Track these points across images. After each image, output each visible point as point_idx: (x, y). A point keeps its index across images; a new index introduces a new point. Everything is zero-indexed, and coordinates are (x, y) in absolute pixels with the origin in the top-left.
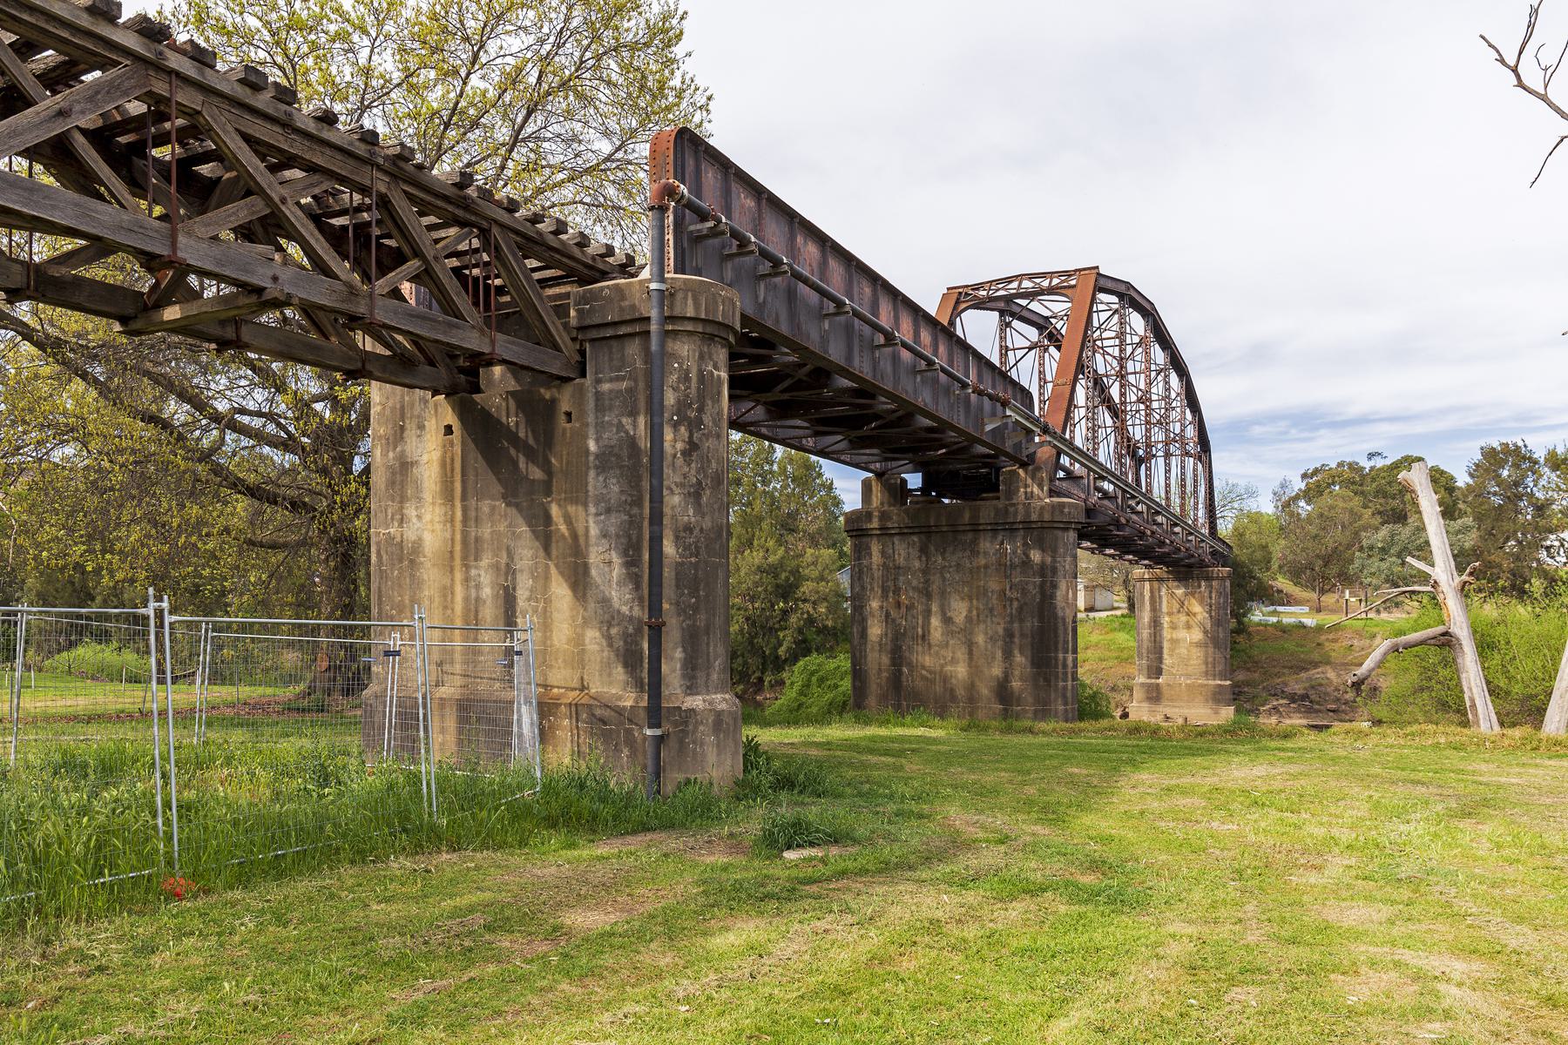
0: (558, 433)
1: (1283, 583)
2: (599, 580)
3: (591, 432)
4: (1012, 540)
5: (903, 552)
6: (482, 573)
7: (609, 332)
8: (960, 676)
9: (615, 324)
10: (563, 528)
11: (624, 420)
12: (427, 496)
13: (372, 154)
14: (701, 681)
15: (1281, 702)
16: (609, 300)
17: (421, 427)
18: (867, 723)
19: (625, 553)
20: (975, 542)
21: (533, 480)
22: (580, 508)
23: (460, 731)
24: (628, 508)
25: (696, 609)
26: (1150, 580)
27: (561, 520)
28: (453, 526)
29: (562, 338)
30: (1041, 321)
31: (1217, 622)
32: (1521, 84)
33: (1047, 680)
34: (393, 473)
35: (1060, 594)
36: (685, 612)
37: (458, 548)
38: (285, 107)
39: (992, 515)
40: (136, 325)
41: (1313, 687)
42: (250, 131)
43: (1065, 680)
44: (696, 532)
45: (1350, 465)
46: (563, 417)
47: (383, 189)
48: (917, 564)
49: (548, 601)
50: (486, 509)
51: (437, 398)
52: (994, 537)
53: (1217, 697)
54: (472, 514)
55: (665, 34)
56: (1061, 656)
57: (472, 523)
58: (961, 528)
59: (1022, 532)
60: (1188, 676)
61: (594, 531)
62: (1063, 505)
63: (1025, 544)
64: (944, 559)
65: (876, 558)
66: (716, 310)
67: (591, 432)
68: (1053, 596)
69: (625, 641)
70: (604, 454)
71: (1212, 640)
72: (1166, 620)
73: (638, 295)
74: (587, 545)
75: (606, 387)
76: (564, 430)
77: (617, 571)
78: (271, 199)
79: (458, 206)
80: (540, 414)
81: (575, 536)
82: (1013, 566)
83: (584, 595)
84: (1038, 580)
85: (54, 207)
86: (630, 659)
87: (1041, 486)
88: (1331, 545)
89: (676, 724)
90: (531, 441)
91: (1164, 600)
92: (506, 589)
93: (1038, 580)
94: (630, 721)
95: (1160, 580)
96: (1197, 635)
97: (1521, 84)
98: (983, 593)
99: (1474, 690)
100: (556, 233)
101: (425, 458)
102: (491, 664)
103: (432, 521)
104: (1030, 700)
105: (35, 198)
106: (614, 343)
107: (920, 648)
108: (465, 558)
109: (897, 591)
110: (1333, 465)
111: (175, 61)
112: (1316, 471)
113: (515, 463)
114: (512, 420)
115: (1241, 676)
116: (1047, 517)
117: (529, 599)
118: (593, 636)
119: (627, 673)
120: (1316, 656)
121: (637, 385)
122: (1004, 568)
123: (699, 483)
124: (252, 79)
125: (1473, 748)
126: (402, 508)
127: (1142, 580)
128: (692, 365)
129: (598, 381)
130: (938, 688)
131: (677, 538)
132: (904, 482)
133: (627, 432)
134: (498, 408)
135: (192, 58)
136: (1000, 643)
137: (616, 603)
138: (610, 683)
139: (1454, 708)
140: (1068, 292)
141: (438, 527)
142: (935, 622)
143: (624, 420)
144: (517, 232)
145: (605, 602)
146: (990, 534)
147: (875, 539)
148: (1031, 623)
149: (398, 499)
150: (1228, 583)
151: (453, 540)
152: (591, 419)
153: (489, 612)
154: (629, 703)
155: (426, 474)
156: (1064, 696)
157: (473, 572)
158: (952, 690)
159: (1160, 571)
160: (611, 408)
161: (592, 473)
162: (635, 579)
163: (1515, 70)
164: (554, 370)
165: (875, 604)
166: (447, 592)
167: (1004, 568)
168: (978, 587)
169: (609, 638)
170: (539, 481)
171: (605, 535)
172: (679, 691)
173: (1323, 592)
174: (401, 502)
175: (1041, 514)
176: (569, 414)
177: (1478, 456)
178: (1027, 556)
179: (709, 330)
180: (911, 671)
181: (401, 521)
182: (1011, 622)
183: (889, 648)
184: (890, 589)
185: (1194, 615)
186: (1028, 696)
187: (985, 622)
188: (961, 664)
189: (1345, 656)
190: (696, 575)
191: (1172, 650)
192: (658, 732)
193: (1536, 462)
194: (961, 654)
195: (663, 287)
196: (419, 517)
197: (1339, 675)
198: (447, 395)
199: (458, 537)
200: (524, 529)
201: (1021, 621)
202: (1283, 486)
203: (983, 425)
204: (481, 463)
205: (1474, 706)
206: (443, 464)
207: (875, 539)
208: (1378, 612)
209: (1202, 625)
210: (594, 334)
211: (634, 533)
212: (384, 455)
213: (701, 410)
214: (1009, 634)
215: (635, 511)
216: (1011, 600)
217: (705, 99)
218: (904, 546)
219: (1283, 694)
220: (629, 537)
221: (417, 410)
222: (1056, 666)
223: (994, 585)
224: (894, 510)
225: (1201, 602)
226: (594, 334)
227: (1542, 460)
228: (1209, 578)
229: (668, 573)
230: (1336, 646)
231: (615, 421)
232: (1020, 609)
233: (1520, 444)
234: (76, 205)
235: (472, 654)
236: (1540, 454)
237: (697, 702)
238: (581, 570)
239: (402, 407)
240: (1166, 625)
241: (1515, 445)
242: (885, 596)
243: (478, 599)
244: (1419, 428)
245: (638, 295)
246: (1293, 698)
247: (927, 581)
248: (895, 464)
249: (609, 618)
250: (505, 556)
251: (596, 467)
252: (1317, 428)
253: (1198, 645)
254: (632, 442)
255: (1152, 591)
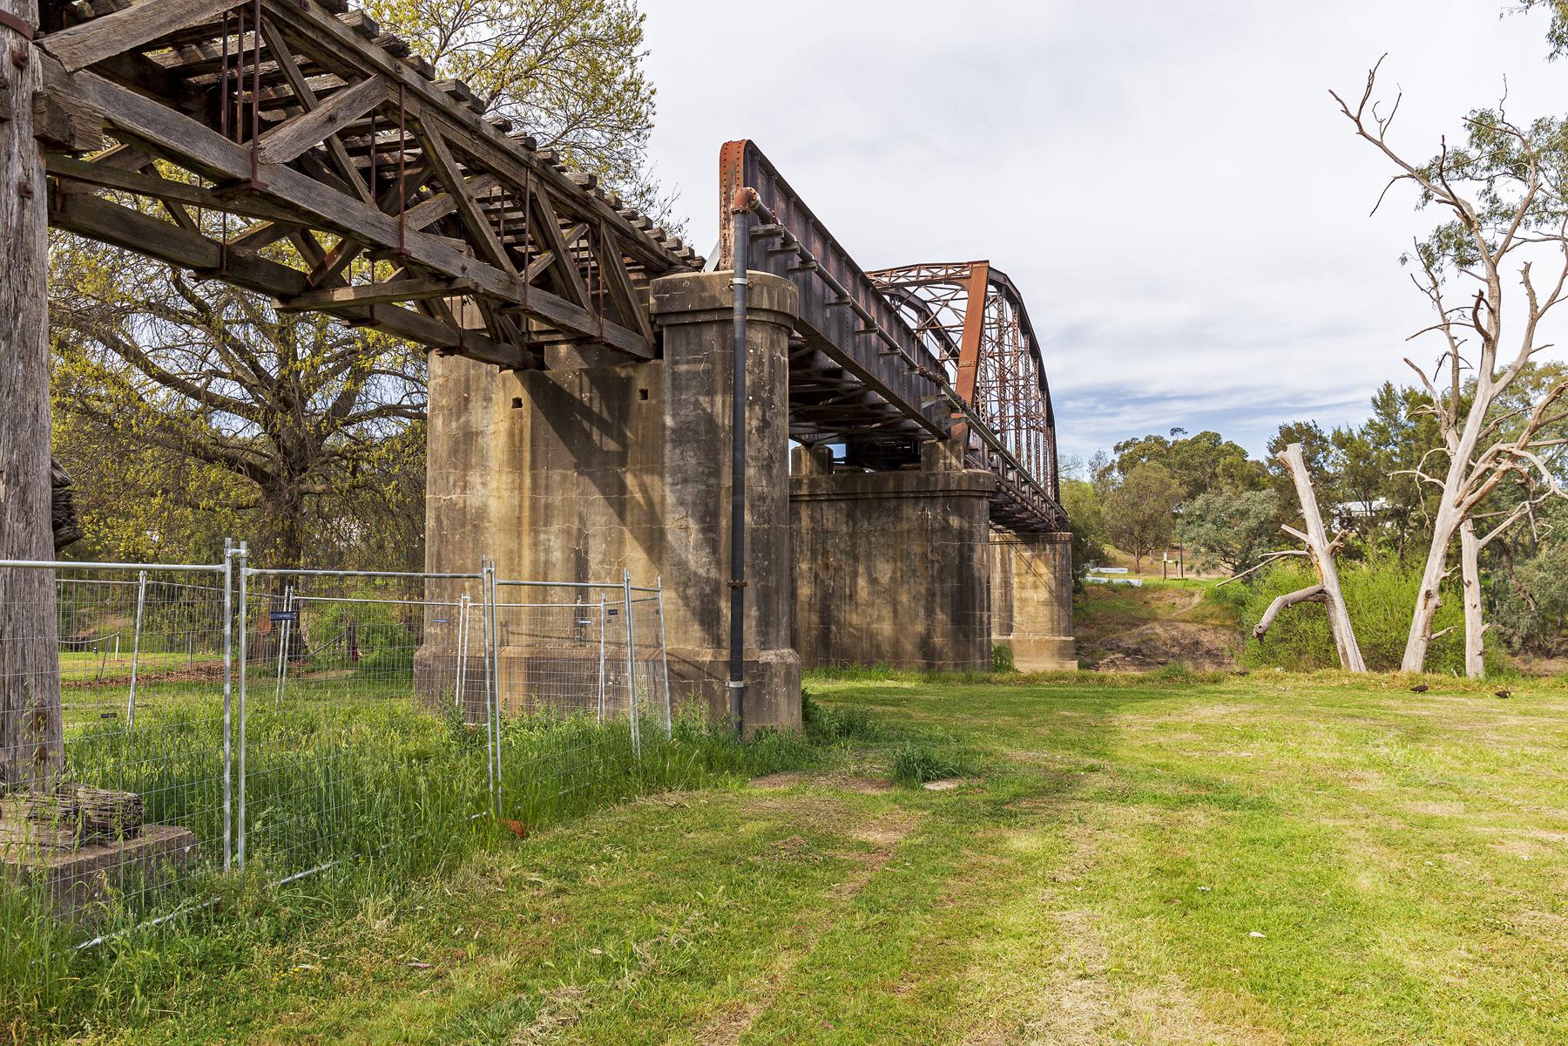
0: (634, 408)
1: (1109, 550)
2: (675, 545)
3: (668, 408)
4: (933, 508)
5: (831, 517)
6: (552, 537)
7: (688, 320)
8: (886, 633)
9: (694, 312)
10: (638, 496)
11: (701, 399)
12: (494, 464)
13: (530, 158)
14: (772, 637)
15: (1117, 655)
16: (690, 290)
17: (488, 399)
18: (837, 678)
19: (702, 520)
20: (898, 508)
21: (608, 452)
22: (656, 478)
23: (529, 688)
24: (705, 478)
25: (768, 572)
26: (1000, 543)
27: (636, 489)
28: (521, 493)
29: (644, 323)
30: (920, 305)
31: (1061, 583)
32: (1362, 132)
33: (967, 637)
34: (456, 442)
35: (976, 556)
36: (758, 572)
37: (526, 513)
38: (475, 116)
39: (915, 483)
40: (295, 304)
41: (1144, 642)
42: (450, 137)
43: (982, 636)
44: (768, 501)
45: (1156, 439)
46: (638, 395)
47: (534, 190)
48: (844, 528)
49: (622, 564)
50: (557, 478)
51: (504, 372)
52: (916, 504)
53: (1063, 652)
54: (543, 482)
55: (626, 36)
56: (978, 613)
57: (542, 491)
58: (885, 495)
59: (941, 500)
60: (1036, 632)
61: (670, 499)
62: (978, 476)
63: (945, 511)
64: (869, 524)
65: (805, 522)
66: (785, 303)
67: (668, 408)
68: (970, 559)
69: (702, 602)
70: (681, 429)
71: (1057, 599)
72: (1015, 581)
73: (718, 287)
74: (663, 512)
75: (683, 368)
76: (640, 406)
77: (694, 535)
78: (461, 197)
79: (580, 205)
80: (617, 393)
81: (650, 503)
82: (934, 531)
83: (660, 558)
84: (957, 544)
85: (324, 203)
86: (707, 617)
87: (958, 458)
88: (1148, 511)
89: (754, 677)
90: (605, 415)
91: (1014, 562)
92: (578, 553)
93: (957, 544)
94: (710, 675)
95: (1009, 543)
96: (1043, 594)
97: (1362, 132)
98: (906, 556)
99: (1345, 640)
100: (643, 229)
101: (492, 428)
102: (561, 623)
103: (498, 489)
104: (951, 655)
105: (312, 195)
106: (692, 330)
107: (847, 608)
108: (534, 523)
109: (825, 554)
110: (1142, 440)
111: (409, 76)
112: (1127, 445)
113: (589, 436)
114: (586, 396)
115: (1081, 633)
116: (965, 487)
117: (602, 562)
118: (668, 599)
119: (703, 630)
120: (1144, 614)
121: (714, 368)
122: (925, 532)
123: (771, 456)
124: (459, 93)
125: (1373, 688)
126: (465, 475)
127: (995, 543)
128: (765, 350)
129: (675, 363)
130: (865, 645)
131: (752, 506)
132: (831, 451)
133: (704, 410)
134: (570, 384)
135: (418, 72)
136: (923, 602)
137: (692, 565)
138: (687, 640)
139: (1327, 655)
140: (964, 282)
141: (505, 494)
142: (862, 582)
143: (701, 399)
144: (617, 228)
145: (681, 565)
146: (912, 501)
147: (804, 505)
148: (951, 584)
149: (461, 466)
150: (1069, 547)
151: (521, 506)
152: (667, 397)
153: (559, 575)
154: (708, 658)
155: (493, 444)
156: (981, 650)
157: (542, 537)
158: (878, 647)
159: (1010, 535)
160: (688, 388)
161: (668, 447)
162: (714, 546)
163: (1357, 121)
164: (637, 352)
165: (804, 566)
166: (513, 556)
167: (925, 532)
168: (902, 550)
169: (685, 598)
170: (613, 452)
171: (681, 503)
172: (754, 646)
173: (1141, 555)
174: (465, 470)
175: (959, 483)
176: (644, 394)
177: (1277, 435)
178: (947, 522)
179: (780, 320)
180: (839, 629)
181: (465, 488)
182: (933, 582)
183: (818, 606)
184: (819, 550)
185: (1041, 575)
186: (949, 652)
187: (908, 583)
188: (887, 622)
189: (1169, 614)
190: (768, 540)
191: (1021, 609)
192: (740, 684)
193: (1325, 441)
194: (887, 612)
195: (745, 282)
196: (484, 484)
197: (1166, 631)
198: (516, 371)
199: (527, 503)
200: (597, 496)
201: (942, 581)
202: (1098, 457)
203: (920, 403)
204: (552, 435)
205: (1345, 653)
206: (511, 434)
207: (804, 505)
208: (1198, 572)
209: (1047, 585)
210: (673, 320)
211: (711, 502)
212: (446, 424)
213: (771, 391)
214: (931, 594)
215: (712, 481)
216: (933, 562)
217: (648, 93)
218: (832, 511)
219: (1118, 649)
220: (707, 505)
221: (484, 382)
222: (974, 623)
223: (916, 548)
224: (823, 478)
225: (1046, 564)
226: (673, 320)
227: (1330, 439)
228: (1053, 542)
229: (747, 540)
230: (1160, 604)
231: (692, 399)
232: (941, 570)
233: (1311, 424)
234: (339, 202)
235: (541, 615)
236: (1328, 434)
237: (769, 656)
238: (657, 535)
239: (467, 380)
240: (1015, 585)
241: (1307, 425)
242: (814, 559)
243: (547, 563)
244: (1207, 406)
245: (718, 287)
246: (1127, 652)
247: (854, 545)
248: (821, 436)
249: (684, 580)
250: (577, 522)
251: (673, 441)
252: (1121, 404)
253: (1044, 603)
254: (710, 419)
255: (1002, 554)
